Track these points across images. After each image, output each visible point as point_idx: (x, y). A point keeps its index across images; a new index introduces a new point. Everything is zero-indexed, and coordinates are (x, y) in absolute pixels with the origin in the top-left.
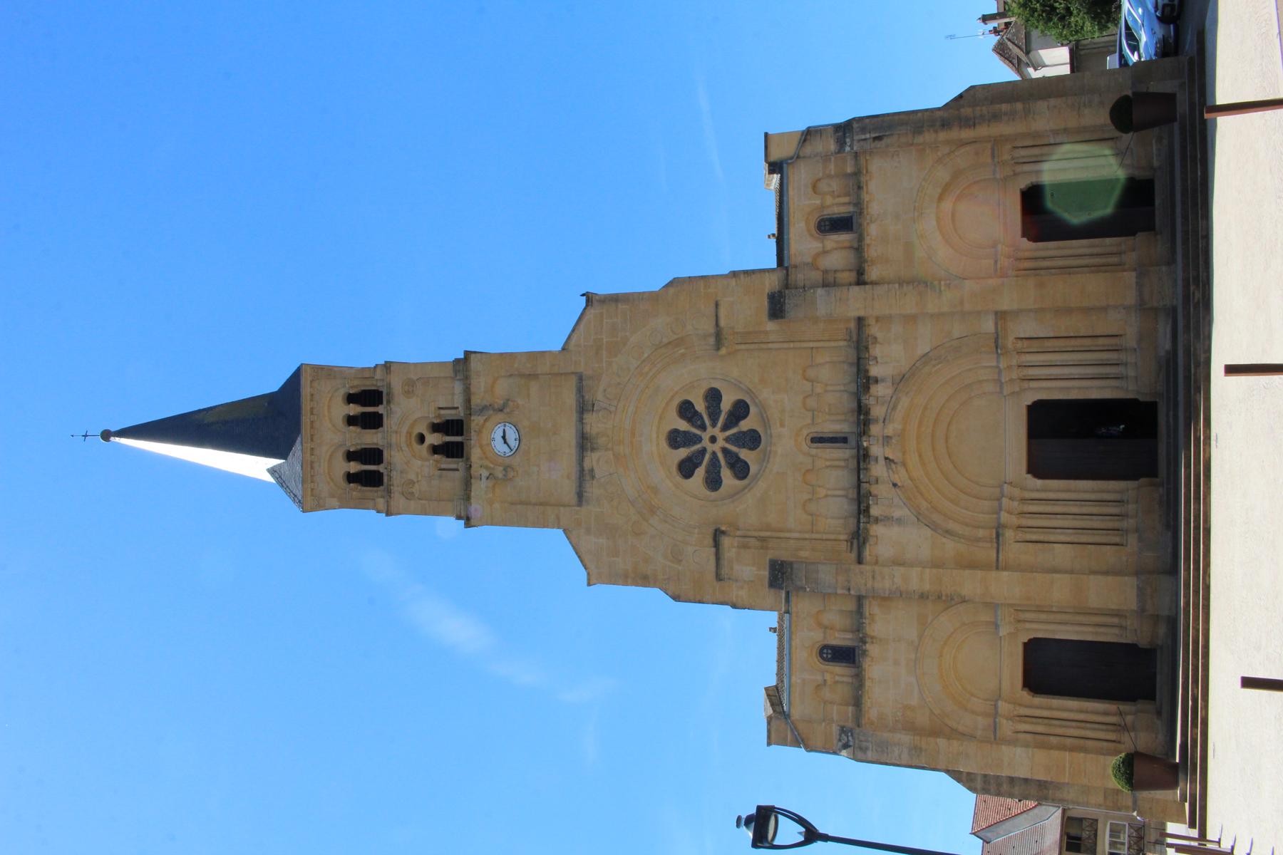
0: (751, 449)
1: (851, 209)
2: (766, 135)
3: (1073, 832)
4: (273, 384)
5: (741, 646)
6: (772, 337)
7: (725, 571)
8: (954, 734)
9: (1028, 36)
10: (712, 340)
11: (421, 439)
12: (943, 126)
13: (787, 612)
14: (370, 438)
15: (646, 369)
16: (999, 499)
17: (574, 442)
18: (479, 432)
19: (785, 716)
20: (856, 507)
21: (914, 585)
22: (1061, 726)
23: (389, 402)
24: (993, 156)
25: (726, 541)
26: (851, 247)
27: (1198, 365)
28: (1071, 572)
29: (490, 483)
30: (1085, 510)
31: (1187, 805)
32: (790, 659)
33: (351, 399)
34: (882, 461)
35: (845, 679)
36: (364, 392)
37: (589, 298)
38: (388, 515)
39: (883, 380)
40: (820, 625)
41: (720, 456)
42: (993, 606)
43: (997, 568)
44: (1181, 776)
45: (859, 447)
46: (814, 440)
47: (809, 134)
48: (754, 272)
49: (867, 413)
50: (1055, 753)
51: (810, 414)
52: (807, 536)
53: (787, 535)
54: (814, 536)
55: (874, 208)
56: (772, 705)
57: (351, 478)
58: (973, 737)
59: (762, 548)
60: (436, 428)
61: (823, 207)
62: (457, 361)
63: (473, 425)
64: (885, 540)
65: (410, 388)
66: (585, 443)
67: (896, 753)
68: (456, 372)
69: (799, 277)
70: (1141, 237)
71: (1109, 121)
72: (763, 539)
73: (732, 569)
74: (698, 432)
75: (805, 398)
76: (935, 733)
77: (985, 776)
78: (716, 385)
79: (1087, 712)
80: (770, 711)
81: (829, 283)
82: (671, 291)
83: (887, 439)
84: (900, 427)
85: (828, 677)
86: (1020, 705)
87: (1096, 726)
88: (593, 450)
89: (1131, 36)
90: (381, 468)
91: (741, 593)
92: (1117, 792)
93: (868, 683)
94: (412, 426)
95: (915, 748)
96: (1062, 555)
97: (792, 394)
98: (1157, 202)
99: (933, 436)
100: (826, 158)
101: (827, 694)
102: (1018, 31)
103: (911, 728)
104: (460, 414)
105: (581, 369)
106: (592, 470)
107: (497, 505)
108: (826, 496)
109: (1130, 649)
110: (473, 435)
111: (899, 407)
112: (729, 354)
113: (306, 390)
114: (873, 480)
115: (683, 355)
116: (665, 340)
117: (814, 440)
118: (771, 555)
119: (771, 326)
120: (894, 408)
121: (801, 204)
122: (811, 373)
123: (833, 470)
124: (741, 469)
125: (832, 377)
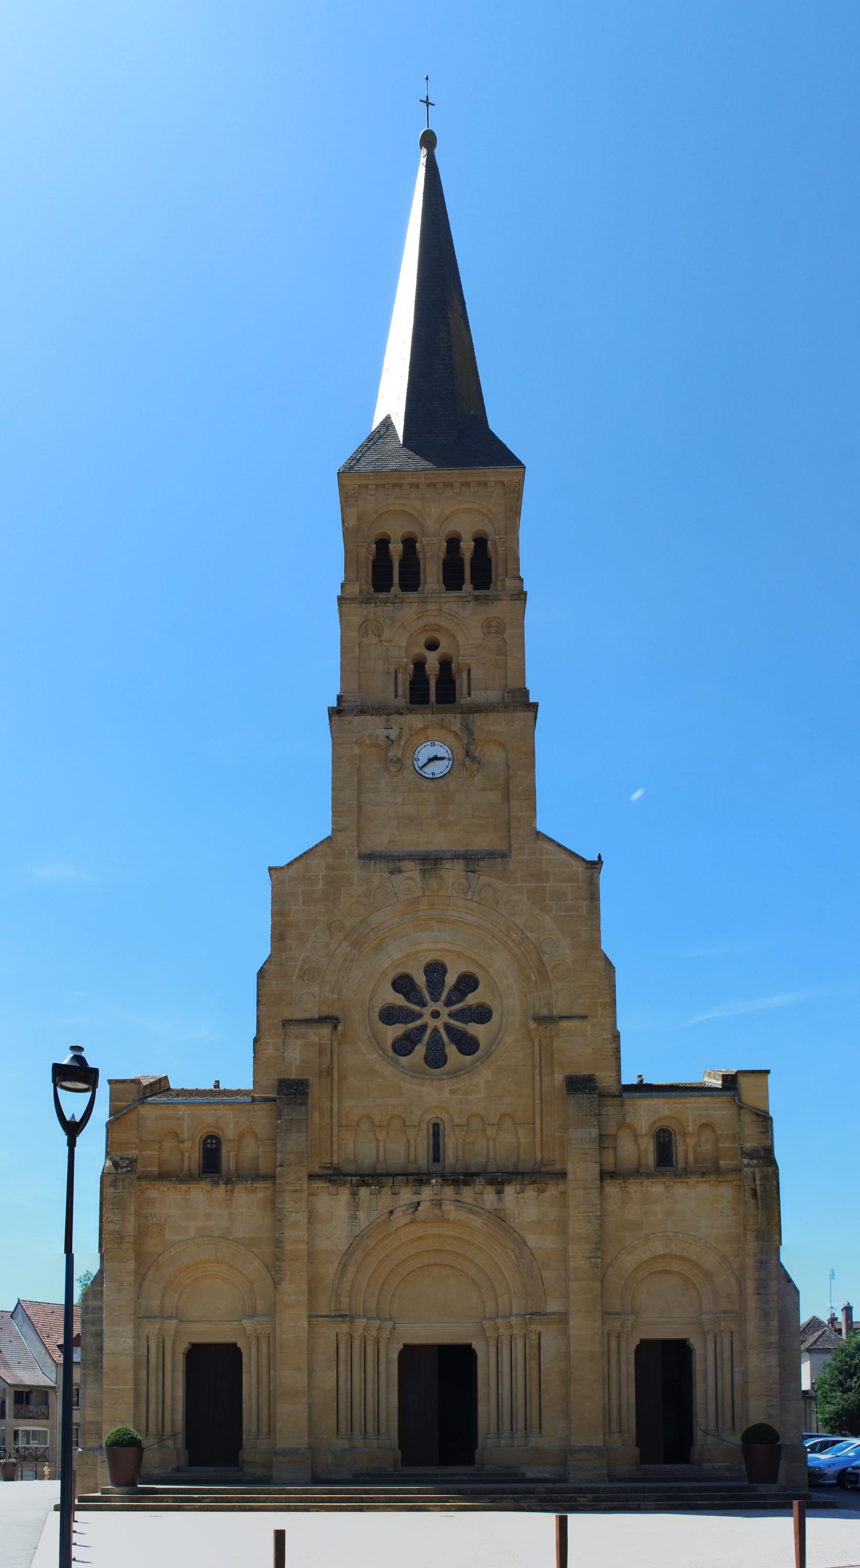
0: (426, 1058)
1: (681, 1165)
2: (768, 1072)
3: (34, 1397)
4: (500, 422)
5: (205, 1043)
6: (546, 1080)
7: (294, 1030)
8: (140, 1277)
9: (826, 1351)
10: (545, 1012)
11: (432, 646)
12: (761, 1262)
13: (254, 1100)
14: (432, 573)
15: (514, 936)
16: (378, 1317)
17: (431, 848)
18: (442, 727)
19: (142, 1100)
20: (367, 1171)
21: (290, 1234)
22: (157, 1380)
23: (477, 598)
24: (725, 1312)
25: (326, 1030)
26: (639, 1165)
27: (515, 1500)
28: (310, 1387)
29: (381, 741)
30: (369, 1399)
31: (99, 1494)
32: (204, 1104)
33: (481, 542)
34: (415, 1198)
35: (186, 1163)
36: (489, 561)
37: (596, 865)
38: (340, 599)
39: (500, 1200)
40: (242, 1135)
41: (418, 1023)
42: (272, 1311)
43: (310, 1316)
44: (126, 1489)
45: (431, 1175)
46: (436, 1126)
47: (764, 1120)
48: (618, 1059)
49: (466, 1183)
50: (130, 1376)
51: (464, 1122)
52: (335, 1120)
53: (335, 1099)
54: (335, 1128)
55: (680, 1190)
56: (152, 1085)
57: (383, 544)
58: (139, 1294)
59: (321, 1071)
60: (445, 665)
61: (685, 1135)
62: (526, 693)
63: (449, 717)
64: (334, 1204)
65: (494, 628)
66: (431, 861)
67: (115, 1218)
68: (513, 692)
69: (610, 1109)
70: (635, 1451)
71: (752, 1423)
72: (330, 1073)
73: (296, 1037)
74: (444, 997)
75: (482, 1117)
76: (140, 1258)
77: (101, 1309)
78: (495, 1017)
79: (173, 1404)
80: (145, 1082)
81: (604, 1142)
82: (601, 964)
83: (438, 1203)
84: (452, 1218)
85: (188, 1144)
86: (174, 1342)
87: (160, 1413)
88: (423, 872)
89: (823, 1447)
90: (395, 589)
91: (271, 1048)
92: (99, 1434)
93: (184, 1187)
94: (448, 632)
95: (122, 1237)
96: (326, 1379)
97: (483, 1100)
98: (668, 1467)
99: (441, 1251)
100: (737, 1138)
101: (169, 1144)
102: (832, 1341)
103: (142, 1233)
104: (463, 700)
105: (515, 857)
106: (400, 871)
107: (356, 750)
108: (377, 1140)
109: (237, 1442)
110: (437, 718)
111: (472, 1216)
112: (529, 1033)
113: (493, 474)
114: (396, 1189)
115: (529, 978)
116: (545, 958)
117: (436, 1126)
118: (314, 1080)
119: (559, 1078)
120: (471, 1211)
121: (690, 1111)
122: (507, 1123)
123: (404, 1147)
124: (403, 1046)
125: (503, 1145)
